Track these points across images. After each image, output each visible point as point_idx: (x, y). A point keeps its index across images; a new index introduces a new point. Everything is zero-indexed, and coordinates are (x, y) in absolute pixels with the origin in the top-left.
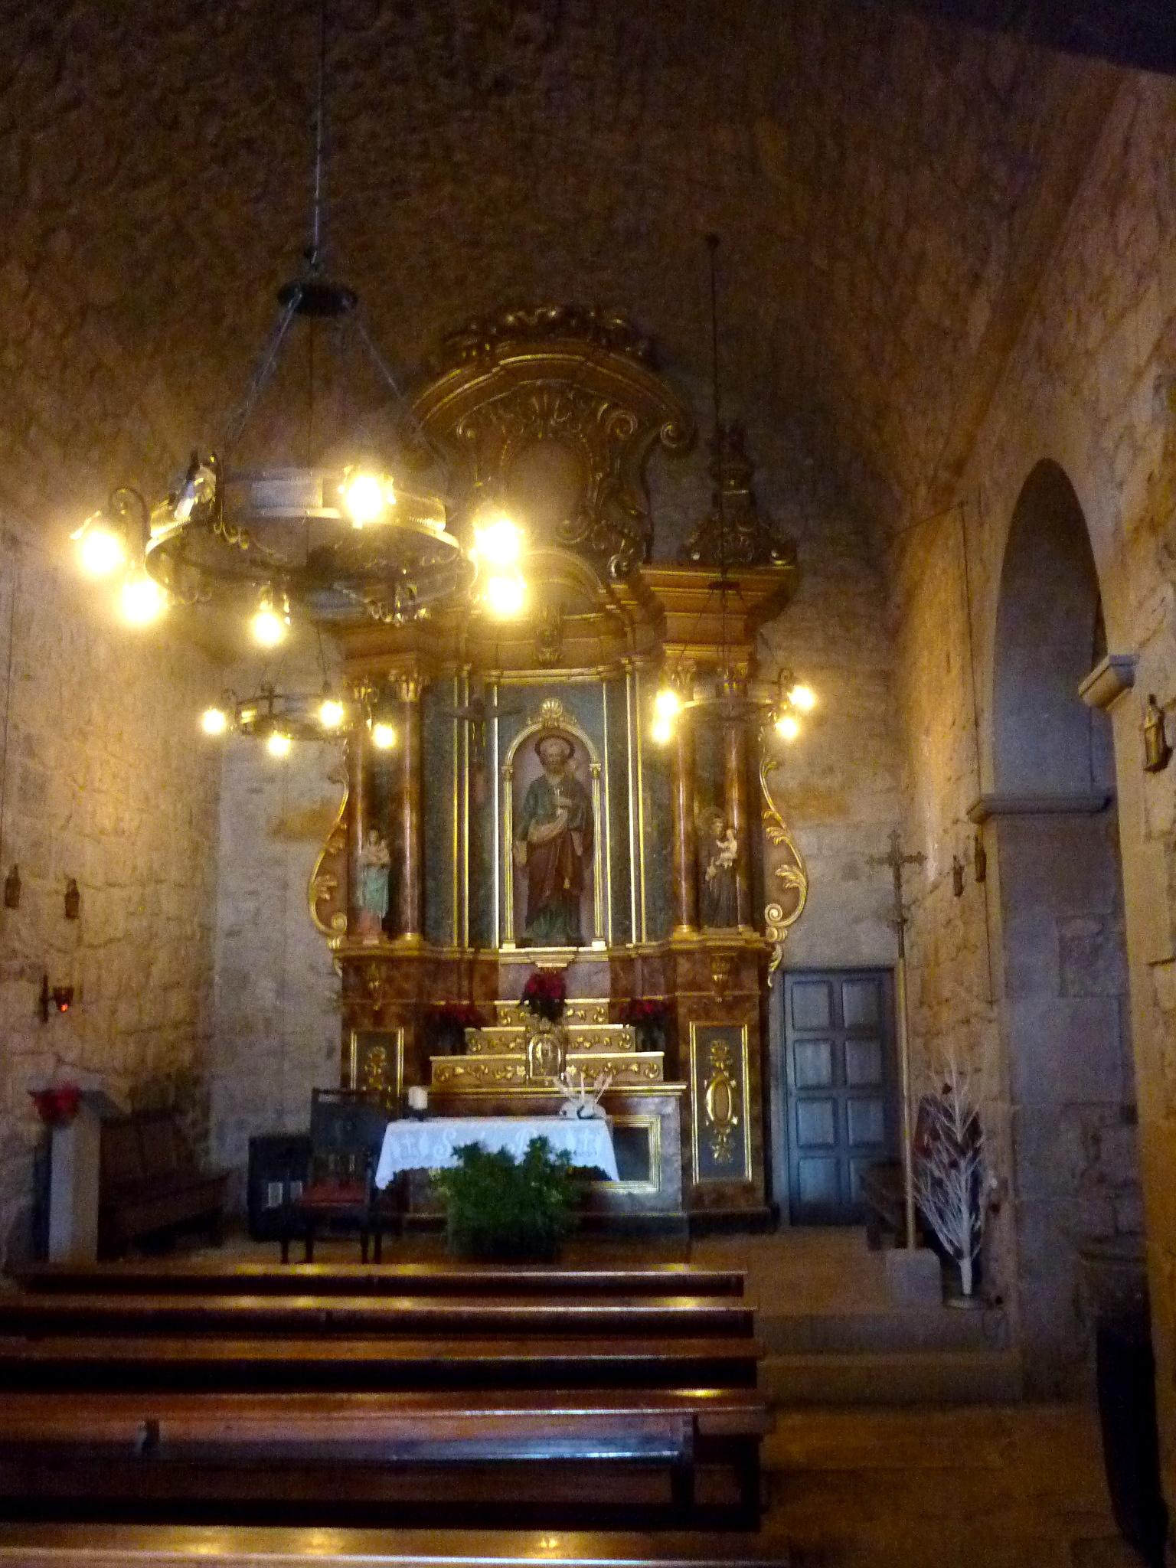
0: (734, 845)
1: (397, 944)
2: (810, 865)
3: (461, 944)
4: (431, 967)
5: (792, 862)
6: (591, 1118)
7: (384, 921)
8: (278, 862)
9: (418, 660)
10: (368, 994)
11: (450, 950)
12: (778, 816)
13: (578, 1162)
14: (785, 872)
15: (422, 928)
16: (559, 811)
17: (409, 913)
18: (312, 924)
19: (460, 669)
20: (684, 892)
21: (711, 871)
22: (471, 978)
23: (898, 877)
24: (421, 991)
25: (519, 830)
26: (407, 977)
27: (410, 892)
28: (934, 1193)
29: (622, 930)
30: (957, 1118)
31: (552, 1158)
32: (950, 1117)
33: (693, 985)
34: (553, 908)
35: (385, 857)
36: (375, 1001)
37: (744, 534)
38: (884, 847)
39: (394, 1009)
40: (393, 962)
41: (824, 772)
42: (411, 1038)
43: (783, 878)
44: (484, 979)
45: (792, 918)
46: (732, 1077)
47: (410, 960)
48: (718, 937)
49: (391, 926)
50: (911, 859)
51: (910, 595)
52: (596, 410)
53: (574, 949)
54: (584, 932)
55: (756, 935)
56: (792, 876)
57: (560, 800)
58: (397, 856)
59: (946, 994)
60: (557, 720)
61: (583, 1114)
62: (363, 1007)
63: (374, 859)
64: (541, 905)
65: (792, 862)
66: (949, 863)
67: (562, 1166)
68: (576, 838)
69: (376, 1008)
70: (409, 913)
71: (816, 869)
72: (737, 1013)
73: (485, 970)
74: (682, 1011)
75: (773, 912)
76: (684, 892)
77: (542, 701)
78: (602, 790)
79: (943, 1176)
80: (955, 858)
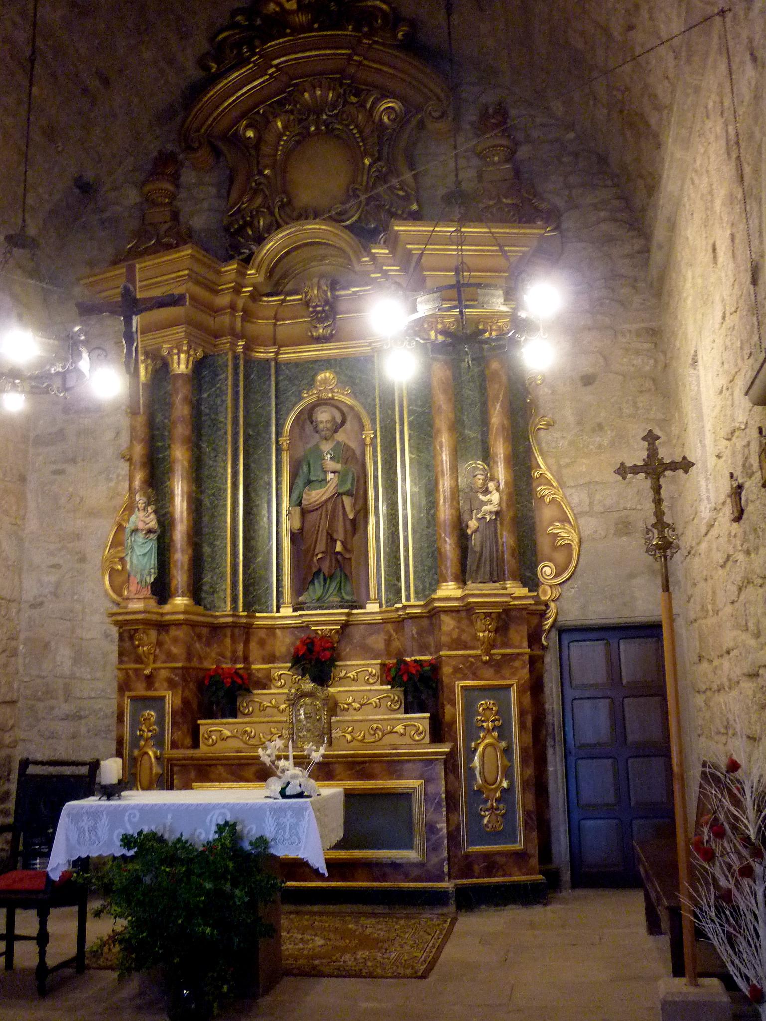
0: (495, 497)
1: (167, 608)
2: (582, 522)
3: (235, 609)
4: (205, 631)
5: (565, 520)
6: (300, 795)
7: (153, 584)
8: (78, 537)
9: (188, 334)
10: (139, 660)
11: (224, 612)
12: (549, 475)
13: (282, 851)
14: (556, 529)
15: (196, 592)
16: (330, 476)
17: (179, 577)
18: (107, 594)
19: (234, 345)
20: (448, 548)
21: (473, 524)
22: (247, 642)
23: (657, 489)
24: (189, 656)
25: (295, 494)
26: (175, 640)
27: (180, 557)
28: (719, 910)
29: (395, 591)
30: (748, 801)
31: (247, 846)
32: (737, 803)
33: (458, 644)
34: (325, 568)
35: (153, 523)
36: (147, 665)
37: (507, 205)
38: (638, 455)
39: (163, 673)
40: (162, 626)
41: (594, 430)
42: (178, 702)
43: (556, 536)
44: (262, 643)
45: (565, 576)
46: (501, 737)
47: (178, 624)
48: (481, 592)
49: (161, 590)
50: (673, 466)
51: (672, 226)
52: (365, 101)
53: (346, 611)
54: (364, 597)
55: (524, 591)
56: (567, 534)
57: (331, 465)
58: (165, 523)
59: (728, 643)
60: (332, 390)
61: (288, 792)
62: (136, 670)
63: (141, 526)
64: (314, 570)
65: (565, 520)
66: (725, 486)
67: (258, 855)
68: (347, 501)
69: (147, 672)
70: (179, 577)
71: (589, 526)
72: (506, 672)
73: (262, 634)
74: (447, 670)
75: (546, 570)
76: (448, 548)
77: (315, 375)
78: (375, 452)
79: (732, 886)
80: (731, 475)
